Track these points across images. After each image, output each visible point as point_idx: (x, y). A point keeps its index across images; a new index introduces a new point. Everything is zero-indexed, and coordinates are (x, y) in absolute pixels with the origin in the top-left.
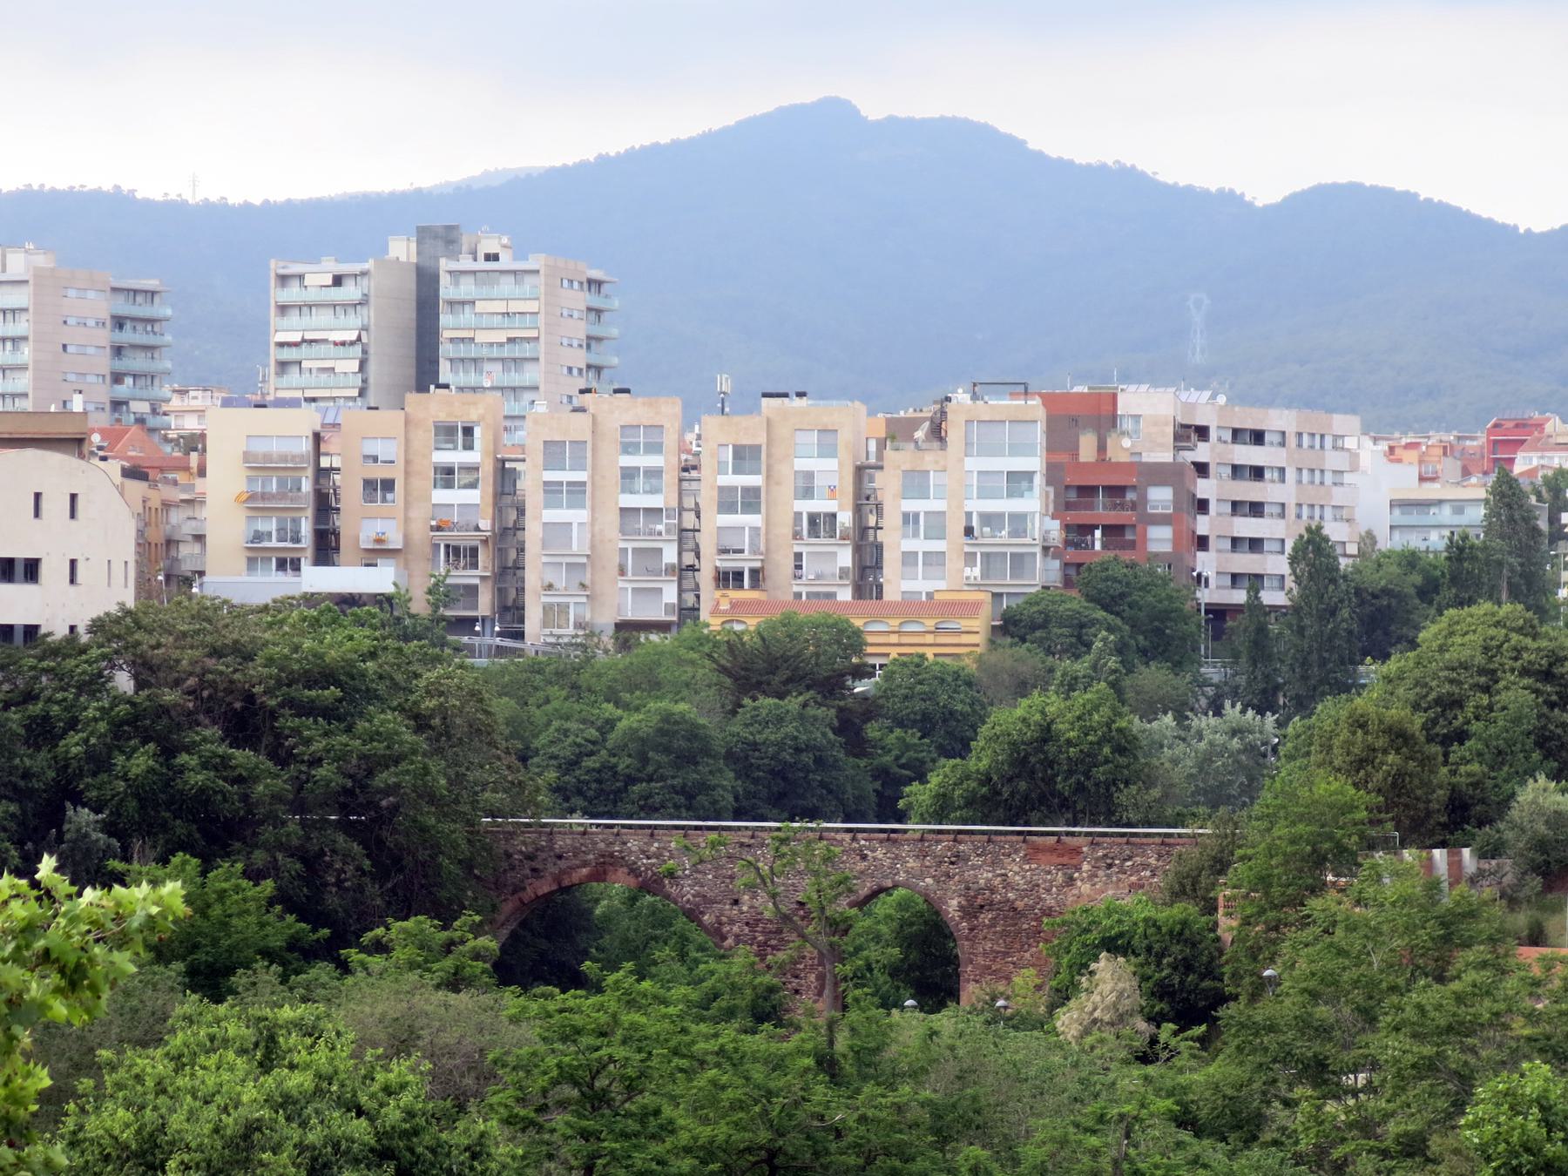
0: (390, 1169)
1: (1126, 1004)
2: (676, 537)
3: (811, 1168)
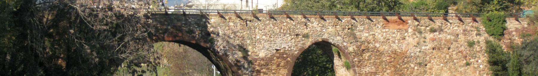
0: (332, 1)
1: (531, 16)
2: (250, 10)
3: (326, 1)
